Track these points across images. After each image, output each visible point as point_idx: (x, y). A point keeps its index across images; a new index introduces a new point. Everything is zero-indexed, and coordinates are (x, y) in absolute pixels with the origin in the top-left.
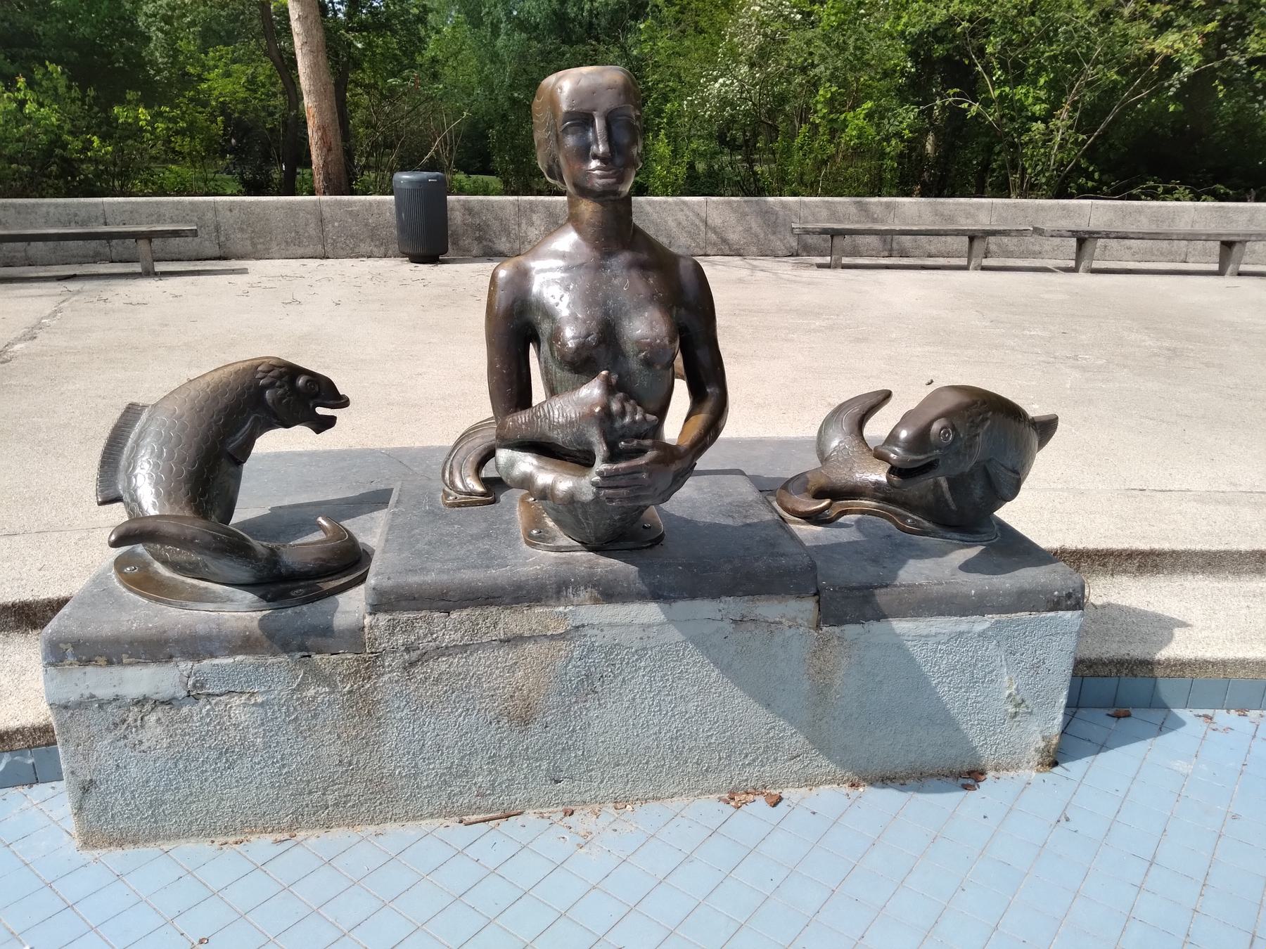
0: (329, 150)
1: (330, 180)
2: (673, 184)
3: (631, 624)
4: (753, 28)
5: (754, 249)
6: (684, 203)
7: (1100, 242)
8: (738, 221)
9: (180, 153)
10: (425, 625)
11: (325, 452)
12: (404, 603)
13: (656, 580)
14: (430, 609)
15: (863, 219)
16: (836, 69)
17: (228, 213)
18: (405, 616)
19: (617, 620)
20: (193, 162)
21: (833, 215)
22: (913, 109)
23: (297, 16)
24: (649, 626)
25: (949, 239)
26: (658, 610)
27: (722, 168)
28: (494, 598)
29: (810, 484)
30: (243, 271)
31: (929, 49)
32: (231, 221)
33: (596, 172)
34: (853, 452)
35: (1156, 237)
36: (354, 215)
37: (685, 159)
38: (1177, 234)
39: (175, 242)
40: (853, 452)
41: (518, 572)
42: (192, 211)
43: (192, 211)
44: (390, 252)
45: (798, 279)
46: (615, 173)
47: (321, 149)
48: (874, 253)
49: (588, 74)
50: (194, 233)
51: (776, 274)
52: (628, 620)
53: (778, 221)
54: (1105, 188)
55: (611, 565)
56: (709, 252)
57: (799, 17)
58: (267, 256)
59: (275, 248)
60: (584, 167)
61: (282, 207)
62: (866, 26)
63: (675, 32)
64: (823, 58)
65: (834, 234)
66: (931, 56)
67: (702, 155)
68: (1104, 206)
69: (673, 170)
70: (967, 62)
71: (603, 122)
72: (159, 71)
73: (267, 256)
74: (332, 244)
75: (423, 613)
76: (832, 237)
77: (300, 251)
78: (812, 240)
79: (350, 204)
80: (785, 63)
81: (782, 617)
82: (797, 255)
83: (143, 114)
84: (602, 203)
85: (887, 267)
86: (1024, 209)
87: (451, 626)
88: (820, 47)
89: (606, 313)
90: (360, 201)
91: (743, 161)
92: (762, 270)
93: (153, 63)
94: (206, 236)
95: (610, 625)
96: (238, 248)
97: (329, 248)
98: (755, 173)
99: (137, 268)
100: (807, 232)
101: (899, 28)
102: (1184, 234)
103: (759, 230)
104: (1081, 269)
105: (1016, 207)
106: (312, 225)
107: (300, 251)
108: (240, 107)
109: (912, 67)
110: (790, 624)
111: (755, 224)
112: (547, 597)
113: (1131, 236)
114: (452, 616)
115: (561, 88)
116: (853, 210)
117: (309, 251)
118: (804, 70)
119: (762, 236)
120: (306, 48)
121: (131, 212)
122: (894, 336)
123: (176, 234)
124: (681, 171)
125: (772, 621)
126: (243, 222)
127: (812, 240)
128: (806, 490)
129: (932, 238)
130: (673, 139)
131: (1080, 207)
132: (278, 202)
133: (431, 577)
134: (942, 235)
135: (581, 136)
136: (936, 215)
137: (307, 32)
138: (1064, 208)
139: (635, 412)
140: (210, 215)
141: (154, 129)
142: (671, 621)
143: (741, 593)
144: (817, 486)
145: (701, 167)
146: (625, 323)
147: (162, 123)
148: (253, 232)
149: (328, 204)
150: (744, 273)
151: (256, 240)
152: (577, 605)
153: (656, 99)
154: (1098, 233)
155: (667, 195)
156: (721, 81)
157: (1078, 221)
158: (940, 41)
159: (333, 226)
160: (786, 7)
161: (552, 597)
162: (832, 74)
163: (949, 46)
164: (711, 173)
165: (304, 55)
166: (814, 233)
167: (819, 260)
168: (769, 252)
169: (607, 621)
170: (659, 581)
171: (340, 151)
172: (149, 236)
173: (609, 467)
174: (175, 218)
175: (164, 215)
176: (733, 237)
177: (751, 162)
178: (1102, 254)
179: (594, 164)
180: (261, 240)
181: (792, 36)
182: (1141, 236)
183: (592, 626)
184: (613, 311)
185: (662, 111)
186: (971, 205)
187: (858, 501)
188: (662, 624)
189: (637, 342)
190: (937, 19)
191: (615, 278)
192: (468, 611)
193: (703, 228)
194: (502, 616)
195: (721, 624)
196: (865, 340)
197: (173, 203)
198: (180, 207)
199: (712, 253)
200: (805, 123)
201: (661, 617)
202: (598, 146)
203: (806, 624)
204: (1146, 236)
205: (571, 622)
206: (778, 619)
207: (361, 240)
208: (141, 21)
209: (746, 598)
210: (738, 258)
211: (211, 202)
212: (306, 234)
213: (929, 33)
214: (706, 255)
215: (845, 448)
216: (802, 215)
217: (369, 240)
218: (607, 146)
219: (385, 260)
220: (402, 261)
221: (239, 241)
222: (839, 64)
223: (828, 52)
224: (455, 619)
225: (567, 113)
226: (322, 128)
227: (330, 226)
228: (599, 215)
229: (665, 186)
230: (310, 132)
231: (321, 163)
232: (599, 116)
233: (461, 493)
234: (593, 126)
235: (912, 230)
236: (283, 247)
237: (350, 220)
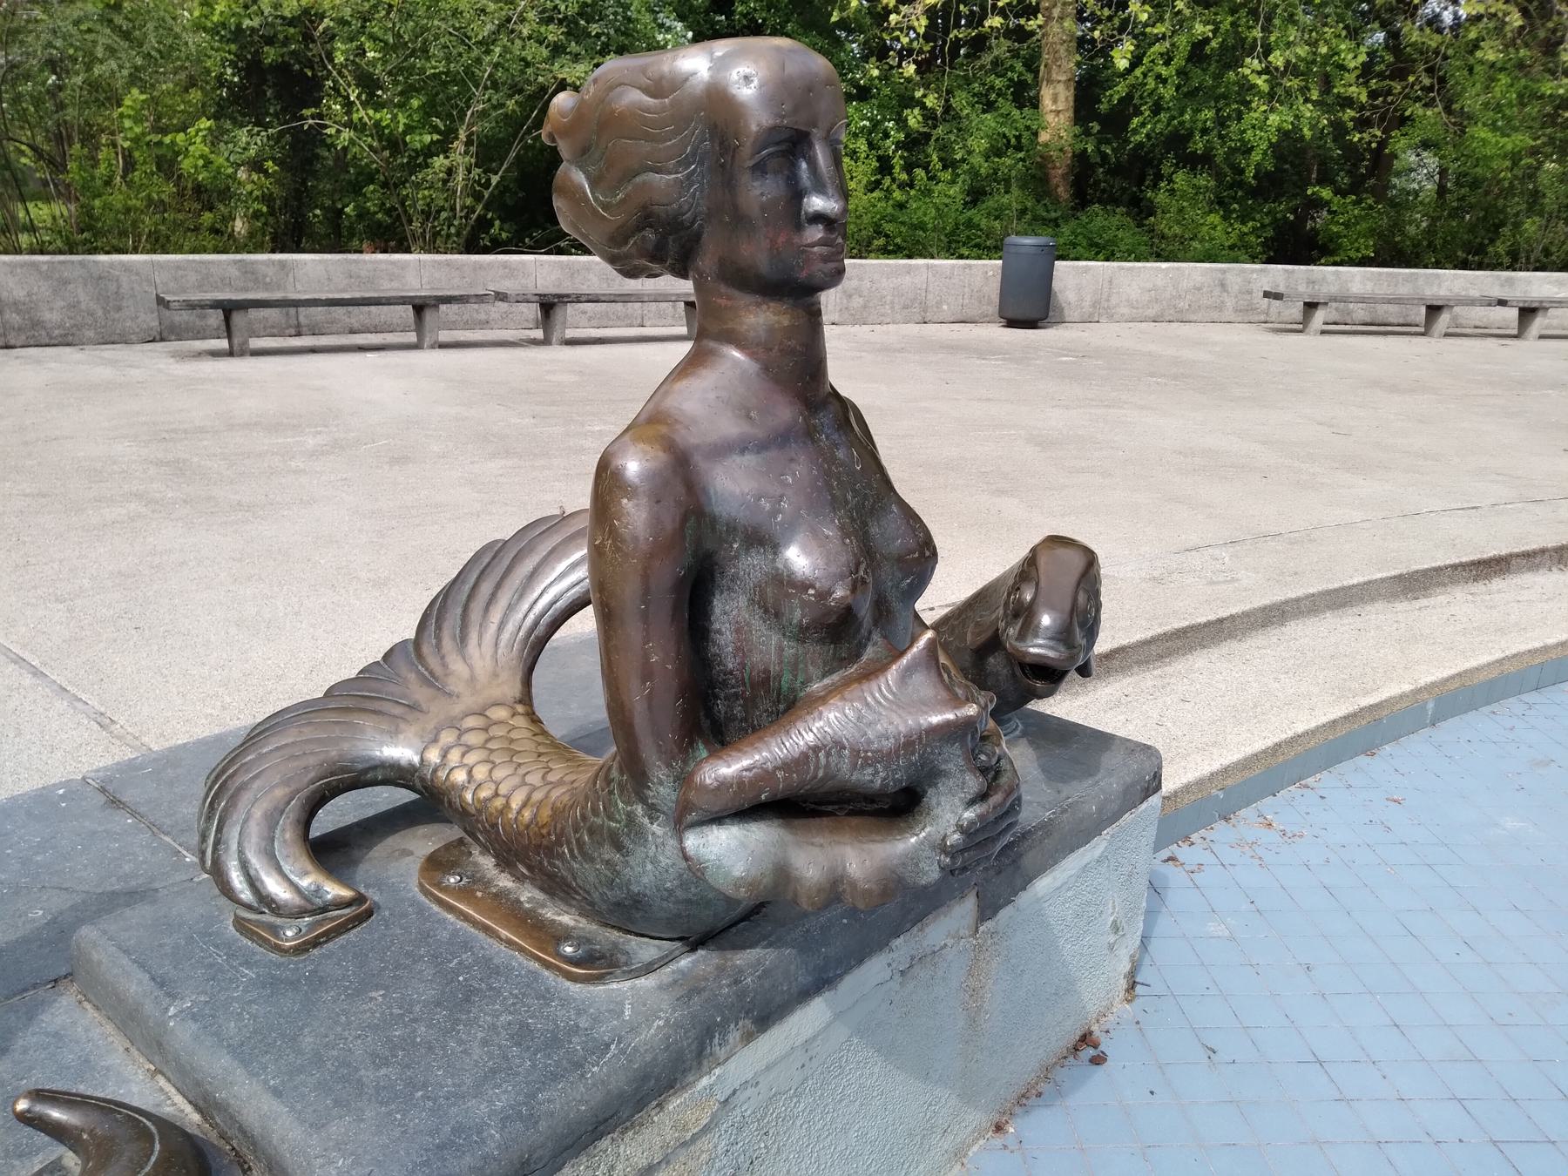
7: (571, 309)
8: (55, 292)
15: (251, 284)
22: (259, 132)
31: (257, 52)
35: (626, 299)
38: (649, 295)
41: (635, 1049)
48: (275, 331)
53: (122, 290)
54: (527, 240)
55: (759, 962)
56: (12, 342)
66: (260, 62)
68: (549, 262)
70: (310, 74)
85: (313, 350)
86: (459, 267)
102: (655, 295)
103: (93, 306)
104: (554, 340)
105: (448, 265)
109: (233, 75)
113: (603, 299)
119: (100, 313)
129: (350, 308)
131: (523, 263)
134: (384, 304)
136: (351, 277)
138: (505, 265)
154: (568, 296)
157: (523, 281)
168: (116, 338)
176: (51, 316)
178: (574, 320)
182: (612, 298)
186: (393, 263)
204: (617, 299)
216: (158, 281)
233: (300, 913)
235: (343, 299)
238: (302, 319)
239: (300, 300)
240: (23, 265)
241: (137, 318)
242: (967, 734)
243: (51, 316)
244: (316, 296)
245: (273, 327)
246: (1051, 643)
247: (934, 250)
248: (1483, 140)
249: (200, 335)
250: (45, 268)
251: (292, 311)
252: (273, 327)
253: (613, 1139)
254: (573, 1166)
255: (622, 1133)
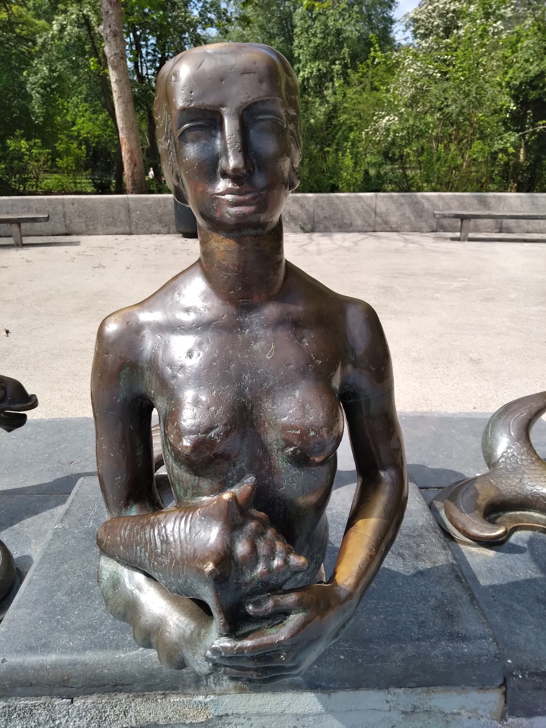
0: (135, 165)
1: (136, 184)
2: (354, 185)
3: (283, 714)
4: (408, 84)
5: (407, 227)
6: (360, 197)
9: (60, 168)
10: (44, 712)
11: (50, 422)
12: (19, 689)
13: (314, 671)
14: (51, 695)
16: (463, 107)
17: (71, 206)
18: (22, 703)
19: (267, 709)
20: (68, 173)
21: (462, 205)
23: (115, 80)
24: (304, 716)
25: (542, 221)
26: (315, 700)
27: (386, 173)
28: (123, 685)
29: (481, 497)
30: (77, 243)
31: (527, 95)
32: (73, 211)
33: (229, 197)
34: (522, 460)
36: (148, 207)
37: (363, 168)
39: (38, 226)
40: (522, 460)
42: (49, 205)
43: (49, 205)
44: (171, 231)
45: (438, 249)
46: (254, 198)
47: (130, 164)
48: (489, 230)
49: (216, 53)
50: (47, 219)
51: (422, 245)
52: (279, 710)
56: (377, 229)
57: (439, 75)
58: (95, 233)
59: (100, 228)
60: (210, 190)
61: (104, 202)
62: (484, 79)
63: (358, 88)
64: (455, 101)
65: (463, 218)
66: (527, 99)
67: (374, 165)
69: (355, 176)
71: (236, 123)
72: (37, 117)
73: (95, 233)
74: (135, 226)
75: (43, 700)
76: (462, 220)
77: (115, 230)
78: (446, 222)
79: (147, 199)
80: (428, 105)
81: (460, 709)
82: (436, 231)
83: (23, 143)
84: (239, 240)
87: (75, 713)
88: (452, 94)
89: (240, 393)
90: (153, 198)
91: (399, 168)
92: (413, 243)
93: (34, 113)
94: (58, 221)
95: (259, 714)
96: (77, 228)
97: (133, 228)
98: (406, 176)
99: (10, 241)
100: (444, 216)
101: (506, 80)
106: (123, 214)
107: (115, 230)
108: (96, 140)
109: (514, 106)
110: (470, 715)
111: (408, 212)
112: (184, 685)
114: (75, 704)
115: (176, 74)
116: (475, 202)
117: (121, 230)
118: (440, 109)
120: (120, 100)
121: (12, 206)
122: (513, 296)
123: (34, 220)
124: (360, 176)
125: (449, 712)
126: (80, 212)
127: (446, 222)
128: (477, 507)
129: (529, 221)
130: (356, 157)
132: (102, 199)
133: (51, 658)
135: (205, 145)
137: (121, 90)
139: (272, 555)
140: (59, 208)
141: (31, 153)
142: (329, 711)
143: (413, 685)
144: (487, 500)
145: (372, 172)
146: (267, 405)
147: (36, 149)
148: (86, 218)
149: (134, 200)
150: (401, 244)
151: (88, 223)
152: (220, 695)
153: (345, 130)
155: (350, 192)
156: (387, 118)
158: (534, 88)
159: (136, 214)
160: (430, 68)
161: (190, 686)
162: (460, 110)
163: (540, 92)
164: (378, 176)
165: (119, 105)
166: (449, 217)
167: (451, 235)
168: (417, 229)
169: (255, 711)
170: (316, 672)
171: (142, 166)
172: (18, 222)
173: (228, 645)
174: (38, 209)
175: (32, 208)
177: (404, 169)
179: (222, 185)
180: (92, 223)
181: (433, 89)
183: (238, 715)
184: (251, 390)
185: (348, 138)
187: (527, 513)
188: (319, 714)
189: (285, 428)
190: (532, 74)
191: (256, 342)
192: (94, 698)
193: (373, 214)
194: (133, 705)
195: (388, 714)
196: (492, 299)
197: (38, 200)
198: (41, 202)
199: (379, 230)
200: (441, 143)
201: (319, 708)
202: (227, 158)
203: (489, 715)
205: (212, 712)
206: (456, 711)
207: (153, 223)
208: (28, 87)
209: (419, 690)
210: (396, 234)
211: (60, 199)
212: (119, 219)
213: (526, 83)
214: (375, 231)
215: (513, 455)
217: (158, 223)
218: (240, 157)
219: (168, 236)
220: (178, 237)
221: (77, 223)
222: (465, 104)
223: (458, 97)
224: (79, 707)
225: (183, 109)
226: (131, 152)
227: (134, 214)
228: (235, 255)
229: (349, 185)
230: (123, 154)
231: (130, 174)
232: (229, 115)
234: (222, 129)
236: (105, 227)
237: (146, 210)
238: (504, 225)
239: (496, 216)
240: (387, 197)
241: (428, 221)
242: (320, 566)
243: (394, 219)
244: (505, 214)
245: (488, 228)
246: (187, 513)
247: (444, 189)
248: (454, 11)
249: (453, 230)
250: (395, 198)
251: (500, 220)
252: (488, 228)
253: (128, 697)
254: (99, 697)
255: (136, 697)
